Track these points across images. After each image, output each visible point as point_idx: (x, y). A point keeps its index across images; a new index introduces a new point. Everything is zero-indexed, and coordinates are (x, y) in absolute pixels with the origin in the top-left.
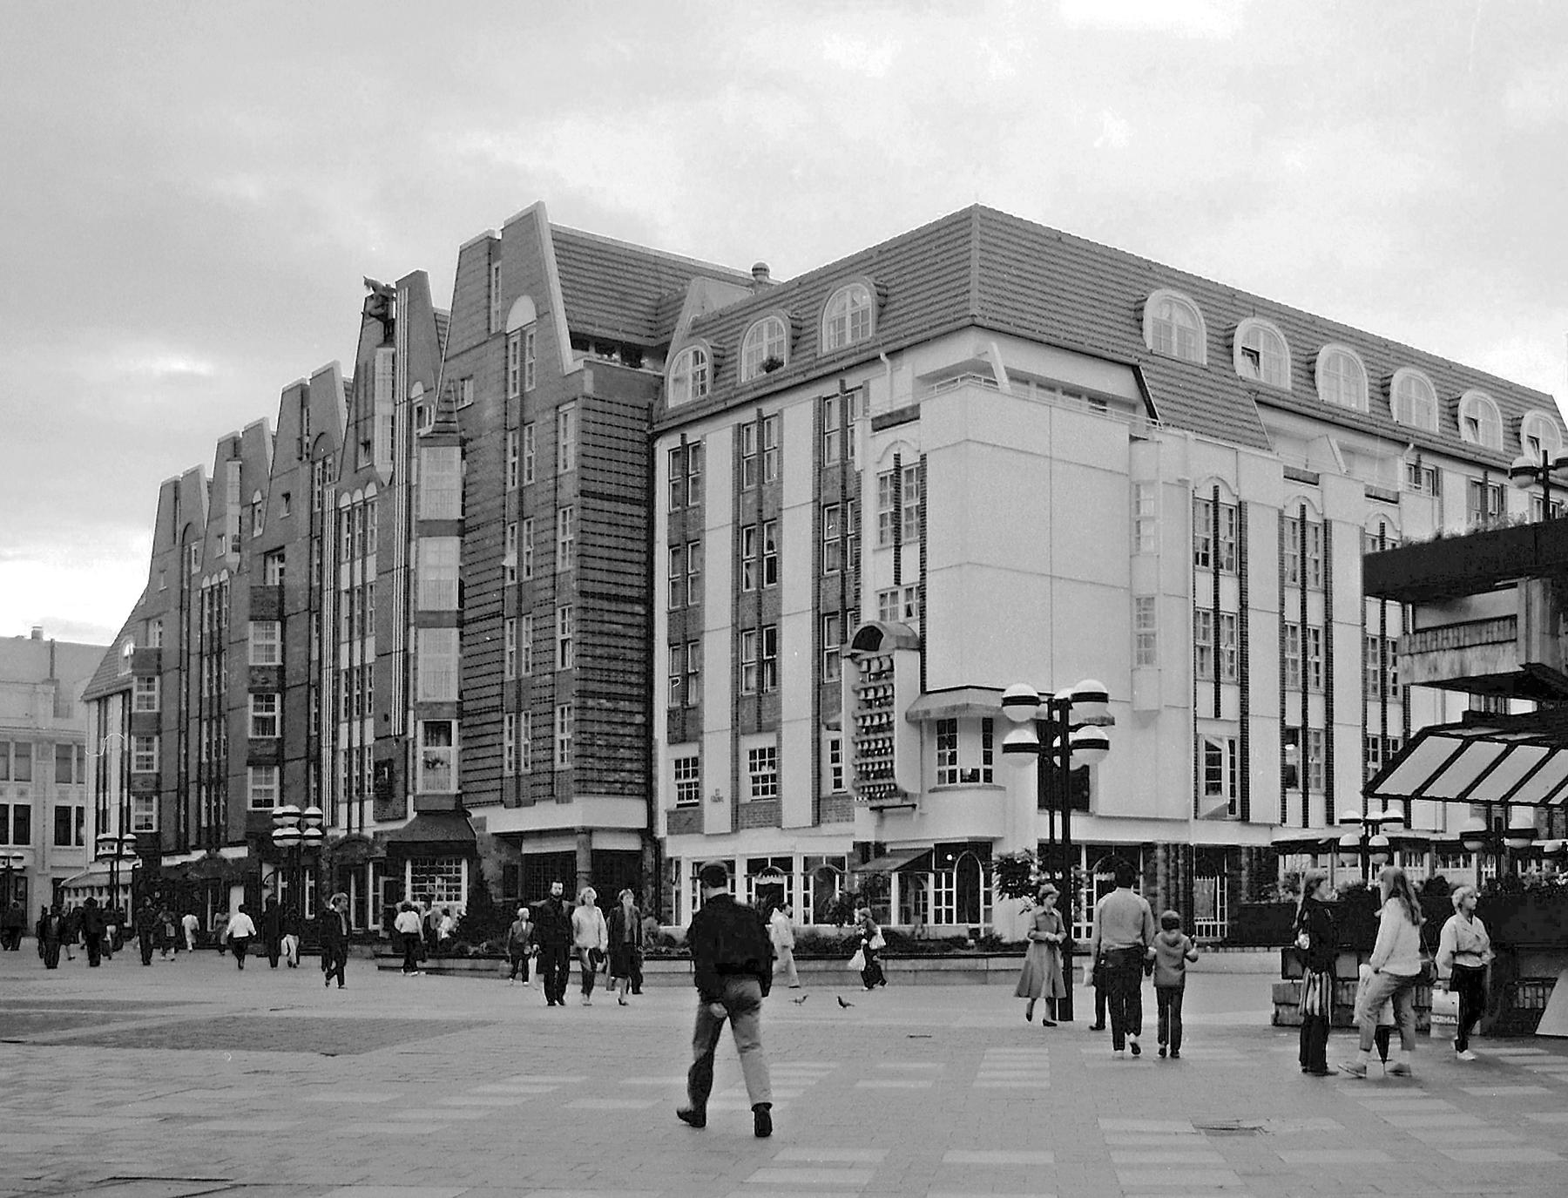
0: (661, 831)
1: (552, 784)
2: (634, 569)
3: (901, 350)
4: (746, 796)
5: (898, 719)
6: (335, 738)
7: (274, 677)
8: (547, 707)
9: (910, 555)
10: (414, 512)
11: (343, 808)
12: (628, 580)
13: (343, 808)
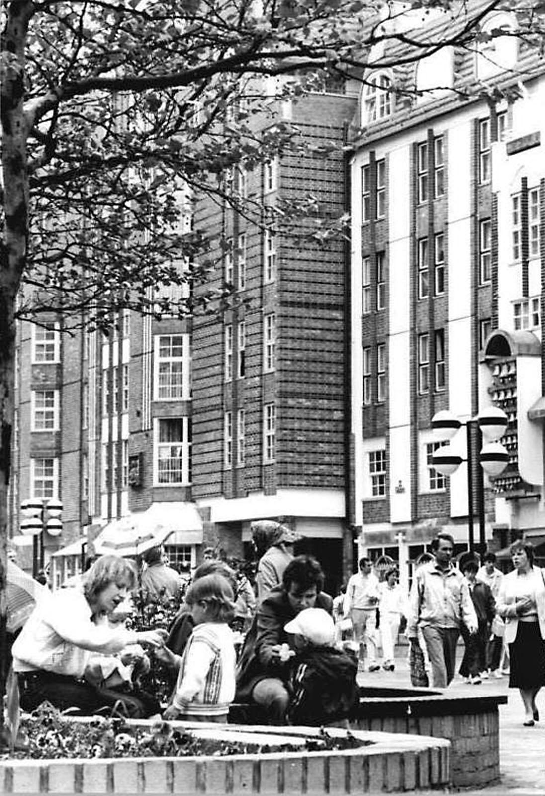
0: (358, 520)
1: (260, 477)
2: (332, 278)
3: (536, 77)
4: (425, 487)
6: (99, 432)
7: (53, 374)
8: (255, 406)
10: (453, 106)
11: (105, 498)
13: (105, 498)
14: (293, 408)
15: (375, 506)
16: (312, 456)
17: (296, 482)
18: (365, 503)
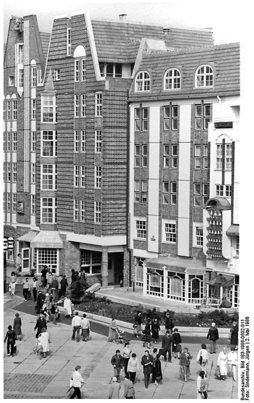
0: (131, 246)
5: (224, 233)
9: (228, 175)
12: (120, 156)
14: (108, 204)
15: (140, 242)
16: (115, 222)
17: (109, 233)
18: (134, 241)
